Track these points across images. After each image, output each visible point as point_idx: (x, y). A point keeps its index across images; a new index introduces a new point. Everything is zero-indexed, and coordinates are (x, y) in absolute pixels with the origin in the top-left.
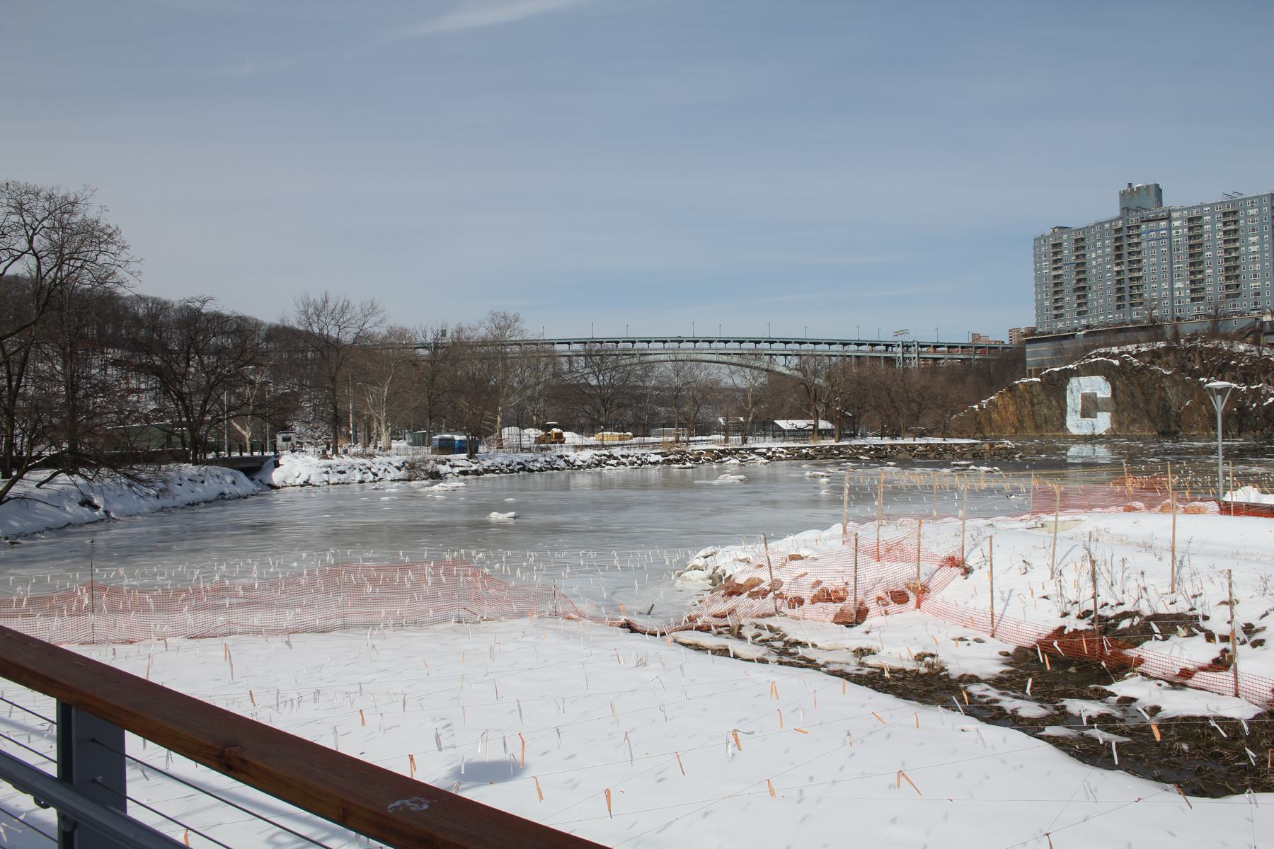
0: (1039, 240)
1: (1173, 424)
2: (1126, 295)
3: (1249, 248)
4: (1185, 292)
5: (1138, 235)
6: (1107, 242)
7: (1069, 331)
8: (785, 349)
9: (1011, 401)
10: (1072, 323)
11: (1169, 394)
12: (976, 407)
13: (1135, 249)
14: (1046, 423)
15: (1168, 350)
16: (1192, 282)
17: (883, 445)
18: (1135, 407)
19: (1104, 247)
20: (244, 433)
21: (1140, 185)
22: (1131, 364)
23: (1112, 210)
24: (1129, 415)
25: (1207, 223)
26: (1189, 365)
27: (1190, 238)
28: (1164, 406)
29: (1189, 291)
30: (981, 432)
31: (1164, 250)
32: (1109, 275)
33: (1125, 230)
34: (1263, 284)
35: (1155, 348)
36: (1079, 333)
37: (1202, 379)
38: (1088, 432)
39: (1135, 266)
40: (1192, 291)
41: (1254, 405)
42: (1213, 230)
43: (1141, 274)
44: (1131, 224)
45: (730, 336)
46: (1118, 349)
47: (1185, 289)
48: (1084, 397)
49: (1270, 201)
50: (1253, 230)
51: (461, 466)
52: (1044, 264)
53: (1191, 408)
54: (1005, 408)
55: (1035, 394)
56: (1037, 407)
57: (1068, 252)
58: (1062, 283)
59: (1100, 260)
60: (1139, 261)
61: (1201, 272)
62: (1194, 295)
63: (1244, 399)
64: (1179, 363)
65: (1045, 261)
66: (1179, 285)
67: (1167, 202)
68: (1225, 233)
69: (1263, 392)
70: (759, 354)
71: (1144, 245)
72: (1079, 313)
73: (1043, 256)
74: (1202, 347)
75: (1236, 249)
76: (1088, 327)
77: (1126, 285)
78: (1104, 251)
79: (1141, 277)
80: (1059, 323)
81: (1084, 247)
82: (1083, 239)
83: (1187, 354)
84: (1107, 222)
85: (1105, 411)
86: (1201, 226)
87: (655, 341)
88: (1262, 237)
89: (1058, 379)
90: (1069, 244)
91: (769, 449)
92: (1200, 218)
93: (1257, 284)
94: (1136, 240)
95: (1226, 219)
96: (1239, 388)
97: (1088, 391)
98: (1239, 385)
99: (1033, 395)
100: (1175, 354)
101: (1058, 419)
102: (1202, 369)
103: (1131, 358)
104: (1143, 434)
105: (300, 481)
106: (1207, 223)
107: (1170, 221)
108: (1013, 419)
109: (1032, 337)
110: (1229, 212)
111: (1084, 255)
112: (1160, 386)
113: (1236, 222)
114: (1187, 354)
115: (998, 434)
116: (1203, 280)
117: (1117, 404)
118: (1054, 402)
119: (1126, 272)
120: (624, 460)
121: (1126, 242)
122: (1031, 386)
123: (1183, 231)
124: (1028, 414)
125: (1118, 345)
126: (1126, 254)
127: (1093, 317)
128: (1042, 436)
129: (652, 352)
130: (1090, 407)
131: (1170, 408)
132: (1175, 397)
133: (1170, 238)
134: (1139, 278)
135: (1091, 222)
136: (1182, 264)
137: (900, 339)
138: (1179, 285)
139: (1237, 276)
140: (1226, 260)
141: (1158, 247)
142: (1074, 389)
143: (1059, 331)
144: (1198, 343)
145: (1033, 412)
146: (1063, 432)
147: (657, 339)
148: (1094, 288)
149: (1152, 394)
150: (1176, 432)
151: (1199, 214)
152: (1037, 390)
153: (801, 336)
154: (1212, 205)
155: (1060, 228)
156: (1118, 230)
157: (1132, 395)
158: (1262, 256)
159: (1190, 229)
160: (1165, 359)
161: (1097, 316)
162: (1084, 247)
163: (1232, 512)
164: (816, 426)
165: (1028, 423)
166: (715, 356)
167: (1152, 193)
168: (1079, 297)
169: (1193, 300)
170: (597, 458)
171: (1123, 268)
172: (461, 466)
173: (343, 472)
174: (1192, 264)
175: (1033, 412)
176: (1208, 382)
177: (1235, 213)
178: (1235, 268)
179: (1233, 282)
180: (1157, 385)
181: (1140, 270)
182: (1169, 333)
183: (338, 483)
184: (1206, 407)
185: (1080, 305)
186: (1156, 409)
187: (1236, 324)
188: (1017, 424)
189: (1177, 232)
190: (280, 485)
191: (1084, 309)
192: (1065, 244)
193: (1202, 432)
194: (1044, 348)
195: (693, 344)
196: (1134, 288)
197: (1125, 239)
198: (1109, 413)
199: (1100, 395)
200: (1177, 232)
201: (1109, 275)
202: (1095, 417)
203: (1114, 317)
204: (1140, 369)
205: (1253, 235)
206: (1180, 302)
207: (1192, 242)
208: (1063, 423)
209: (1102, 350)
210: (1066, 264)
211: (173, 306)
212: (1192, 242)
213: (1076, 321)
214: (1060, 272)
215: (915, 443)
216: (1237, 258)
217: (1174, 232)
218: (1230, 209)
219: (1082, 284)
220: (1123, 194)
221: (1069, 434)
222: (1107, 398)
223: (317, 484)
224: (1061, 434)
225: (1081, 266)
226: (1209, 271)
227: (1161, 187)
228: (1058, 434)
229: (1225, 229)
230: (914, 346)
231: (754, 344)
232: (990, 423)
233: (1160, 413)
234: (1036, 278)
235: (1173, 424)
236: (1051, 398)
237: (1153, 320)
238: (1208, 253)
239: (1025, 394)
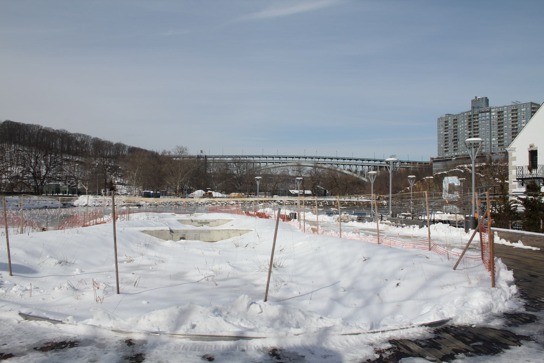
0: (440, 119)
3: (522, 125)
4: (496, 142)
5: (478, 118)
6: (465, 121)
7: (450, 158)
8: (368, 163)
9: (421, 186)
10: (452, 154)
11: (483, 184)
12: (408, 188)
13: (476, 124)
15: (487, 166)
16: (499, 138)
17: (331, 201)
19: (464, 123)
20: (86, 188)
21: (480, 97)
22: (468, 172)
23: (468, 107)
25: (505, 114)
27: (498, 120)
29: (497, 142)
31: (488, 125)
32: (466, 134)
33: (472, 116)
35: (481, 165)
36: (453, 159)
37: (496, 179)
39: (476, 131)
40: (499, 142)
43: (478, 134)
45: (320, 156)
46: (467, 165)
47: (496, 141)
48: (450, 185)
49: (530, 105)
50: (524, 117)
51: (150, 202)
52: (441, 129)
55: (431, 183)
58: (448, 137)
59: (463, 128)
60: (478, 129)
61: (502, 134)
62: (499, 144)
66: (494, 139)
67: (490, 105)
68: (513, 118)
70: (332, 164)
71: (480, 122)
72: (454, 150)
73: (441, 126)
74: (500, 165)
75: (517, 125)
76: (456, 156)
80: (446, 154)
83: (493, 168)
84: (465, 112)
86: (503, 115)
87: (289, 157)
89: (440, 177)
90: (451, 121)
91: (281, 201)
92: (502, 112)
94: (477, 120)
95: (513, 112)
97: (451, 183)
99: (430, 184)
100: (489, 168)
103: (469, 169)
105: (84, 204)
106: (505, 114)
107: (491, 113)
109: (434, 161)
110: (514, 110)
111: (457, 126)
112: (479, 181)
113: (517, 114)
114: (493, 168)
116: (503, 137)
118: (438, 187)
119: (473, 133)
120: (219, 203)
121: (472, 121)
123: (496, 117)
125: (467, 164)
126: (472, 126)
127: (460, 152)
129: (287, 162)
130: (452, 188)
133: (490, 120)
135: (459, 113)
136: (495, 131)
138: (494, 139)
141: (486, 124)
142: (446, 181)
143: (446, 157)
147: (290, 157)
148: (460, 140)
151: (502, 110)
152: (431, 181)
153: (350, 157)
154: (507, 107)
155: (448, 114)
156: (470, 116)
159: (499, 116)
160: (485, 170)
161: (461, 151)
162: (457, 123)
163: (87, 194)
164: (304, 192)
167: (484, 101)
168: (454, 143)
169: (499, 146)
170: (208, 202)
171: (471, 132)
172: (150, 202)
173: (101, 202)
174: (499, 131)
177: (516, 110)
180: (478, 181)
181: (478, 133)
182: (488, 159)
183: (98, 206)
185: (455, 147)
189: (493, 117)
190: (76, 205)
191: (456, 148)
192: (450, 121)
194: (439, 164)
195: (305, 159)
197: (472, 120)
199: (456, 184)
200: (493, 117)
201: (466, 134)
205: (524, 119)
206: (494, 147)
209: (461, 166)
210: (450, 130)
211: (91, 138)
212: (499, 122)
214: (447, 133)
215: (344, 200)
216: (517, 129)
217: (492, 117)
218: (515, 108)
219: (456, 138)
220: (473, 101)
223: (90, 206)
225: (455, 130)
227: (488, 98)
229: (512, 116)
230: (398, 162)
231: (330, 160)
234: (438, 135)
236: (437, 185)
237: (482, 154)
238: (506, 126)
239: (427, 183)
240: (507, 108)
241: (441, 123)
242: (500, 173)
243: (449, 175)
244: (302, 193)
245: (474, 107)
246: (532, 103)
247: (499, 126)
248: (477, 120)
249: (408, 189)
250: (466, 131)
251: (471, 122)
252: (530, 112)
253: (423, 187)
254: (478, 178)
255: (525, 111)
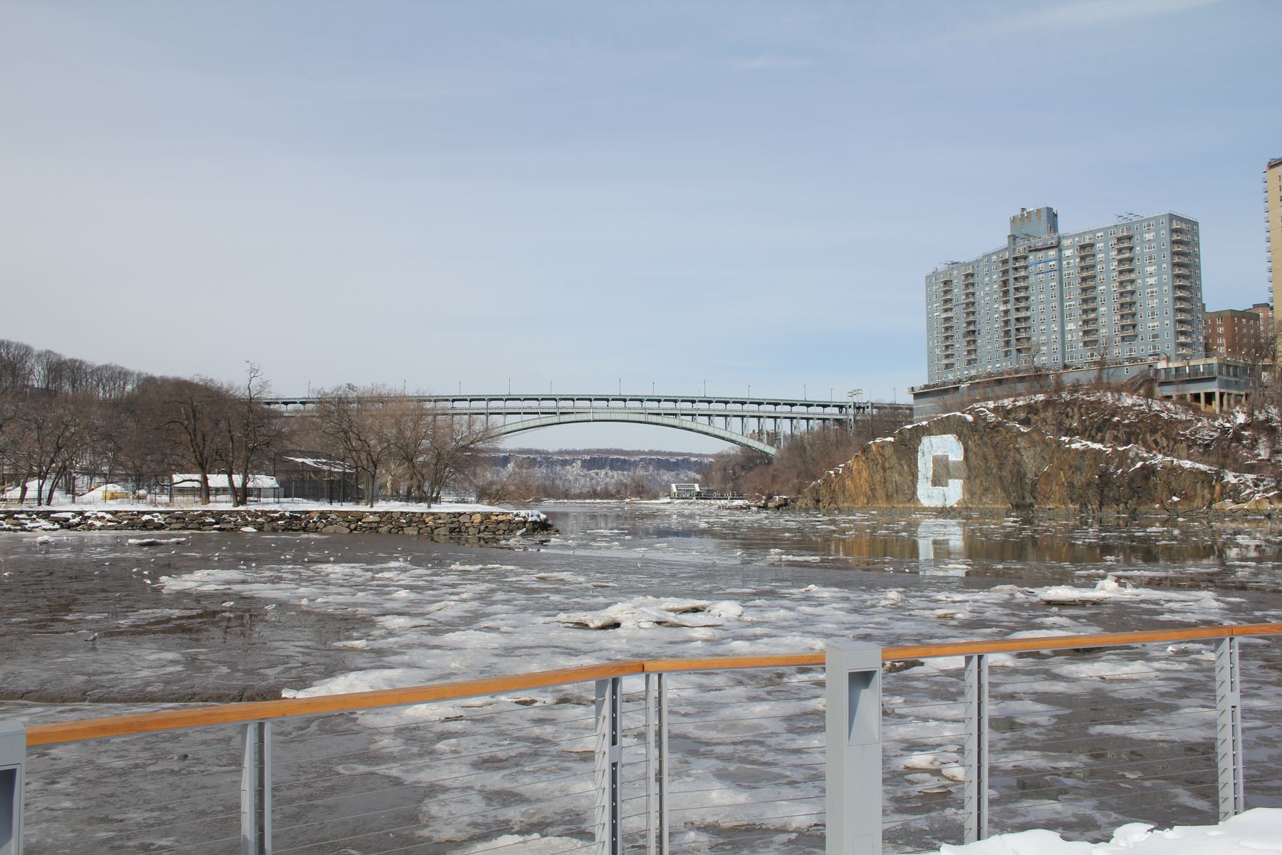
1: (1027, 495)
2: (1013, 339)
5: (1026, 268)
6: (995, 277)
7: (955, 383)
8: (742, 411)
12: (832, 472)
14: (897, 492)
15: (1047, 404)
16: (1086, 322)
18: (988, 474)
22: (985, 419)
24: (981, 484)
26: (1067, 422)
28: (1019, 472)
29: (1081, 334)
30: (836, 503)
31: (1053, 284)
32: (996, 316)
33: (1011, 261)
34: (1162, 323)
35: (1032, 401)
37: (1063, 438)
38: (939, 504)
39: (1022, 304)
40: (1086, 333)
41: (1120, 471)
42: (1106, 259)
43: (1029, 314)
44: (1017, 255)
49: (1168, 222)
50: (1150, 258)
53: (1049, 474)
54: (859, 473)
55: (887, 457)
56: (888, 472)
57: (958, 292)
60: (1027, 298)
61: (1094, 310)
62: (1087, 339)
63: (1107, 464)
64: (1056, 419)
65: (936, 302)
66: (1071, 326)
67: (1062, 229)
68: (1120, 261)
69: (1131, 454)
71: (1032, 279)
74: (1083, 399)
75: (1132, 281)
76: (971, 378)
77: (1012, 328)
78: (991, 288)
79: (1029, 318)
81: (973, 285)
82: (972, 275)
83: (1066, 408)
84: (994, 253)
85: (957, 478)
86: (1094, 255)
88: (1160, 267)
92: (1092, 245)
93: (1156, 324)
96: (1104, 449)
97: (939, 453)
98: (1105, 447)
100: (1054, 409)
101: (909, 487)
102: (1080, 428)
103: (987, 412)
104: (996, 506)
107: (1060, 251)
108: (866, 487)
111: (973, 294)
112: (1015, 448)
115: (851, 505)
117: (970, 469)
119: (1013, 311)
121: (1012, 275)
122: (883, 447)
124: (880, 481)
126: (1012, 291)
128: (893, 507)
131: (1025, 474)
132: (1032, 461)
133: (1060, 270)
134: (1026, 319)
136: (1073, 301)
137: (851, 401)
138: (1071, 326)
139: (1133, 315)
140: (1122, 294)
142: (926, 450)
144: (1078, 395)
145: (885, 479)
146: (914, 503)
149: (1006, 457)
150: (1032, 505)
151: (1091, 241)
156: (1005, 262)
157: (985, 458)
158: (1161, 289)
159: (1083, 258)
165: (880, 492)
166: (643, 416)
169: (1085, 344)
174: (1085, 301)
175: (885, 479)
176: (1070, 442)
177: (1130, 238)
178: (1132, 304)
179: (1129, 322)
180: (1011, 446)
181: (1027, 309)
184: (1064, 474)
186: (1009, 476)
187: (1128, 373)
188: (870, 493)
189: (1068, 263)
193: (1059, 506)
196: (1022, 330)
197: (1011, 272)
198: (961, 481)
199: (952, 458)
200: (1068, 263)
202: (947, 485)
203: (1005, 365)
204: (994, 426)
206: (1072, 347)
207: (1085, 274)
208: (914, 493)
213: (966, 372)
214: (949, 314)
216: (1132, 293)
217: (1065, 263)
218: (1125, 234)
219: (972, 328)
220: (1014, 220)
221: (920, 506)
222: (959, 462)
224: (912, 506)
226: (1102, 309)
227: (1054, 211)
228: (908, 505)
229: (1119, 257)
232: (844, 492)
233: (1014, 480)
235: (1027, 495)
236: (903, 462)
237: (1037, 369)
240: (1106, 233)
241: (934, 288)
242: (1082, 422)
243: (934, 432)
244: (197, 485)
245: (1014, 236)
246: (1172, 217)
247: (1084, 285)
248: (1023, 273)
249: (831, 475)
250: (996, 306)
251: (1008, 280)
252: (1169, 243)
253: (869, 468)
254: (1011, 437)
255: (1154, 240)
